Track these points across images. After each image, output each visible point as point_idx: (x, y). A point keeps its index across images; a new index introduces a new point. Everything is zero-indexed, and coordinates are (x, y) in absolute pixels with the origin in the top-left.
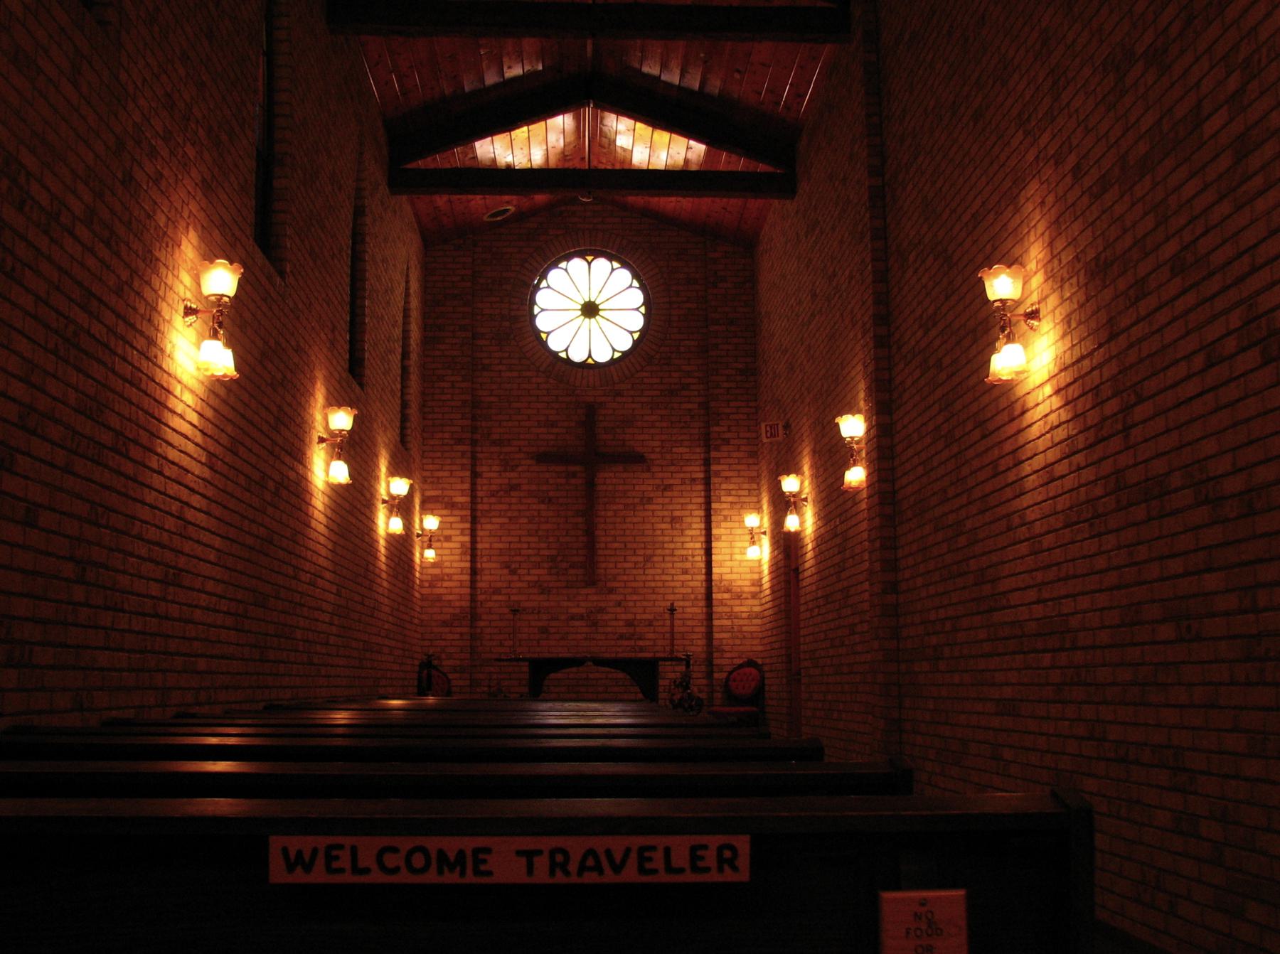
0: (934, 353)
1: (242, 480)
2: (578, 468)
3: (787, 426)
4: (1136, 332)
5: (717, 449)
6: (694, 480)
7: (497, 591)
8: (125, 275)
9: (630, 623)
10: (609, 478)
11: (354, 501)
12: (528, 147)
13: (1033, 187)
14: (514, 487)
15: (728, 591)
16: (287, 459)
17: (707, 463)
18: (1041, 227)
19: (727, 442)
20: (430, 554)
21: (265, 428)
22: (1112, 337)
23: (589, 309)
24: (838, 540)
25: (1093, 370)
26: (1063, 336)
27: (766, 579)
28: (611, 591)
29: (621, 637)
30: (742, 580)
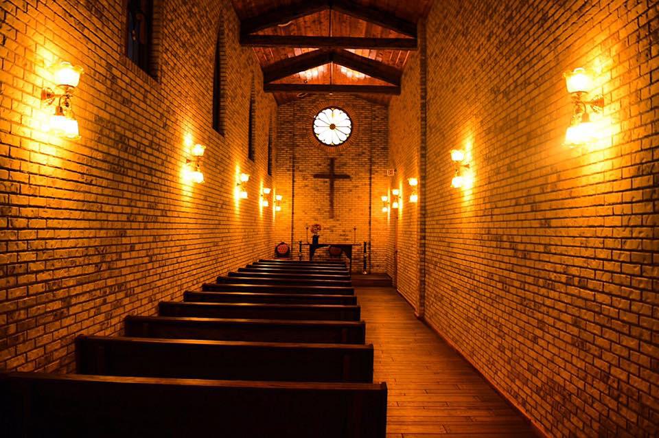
0: (434, 171)
1: (209, 208)
2: (327, 180)
3: (395, 171)
4: (497, 185)
5: (374, 174)
6: (365, 184)
7: (300, 220)
8: (164, 158)
9: (344, 231)
10: (338, 183)
11: (250, 206)
12: (312, 74)
13: (469, 122)
14: (306, 186)
15: (376, 221)
16: (225, 195)
17: (370, 178)
18: (471, 137)
19: (377, 172)
20: (279, 209)
21: (217, 188)
22: (490, 183)
23: (333, 126)
24: (409, 215)
25: (483, 191)
26: (476, 177)
27: (389, 218)
28: (338, 220)
29: (341, 235)
30: (381, 218)
